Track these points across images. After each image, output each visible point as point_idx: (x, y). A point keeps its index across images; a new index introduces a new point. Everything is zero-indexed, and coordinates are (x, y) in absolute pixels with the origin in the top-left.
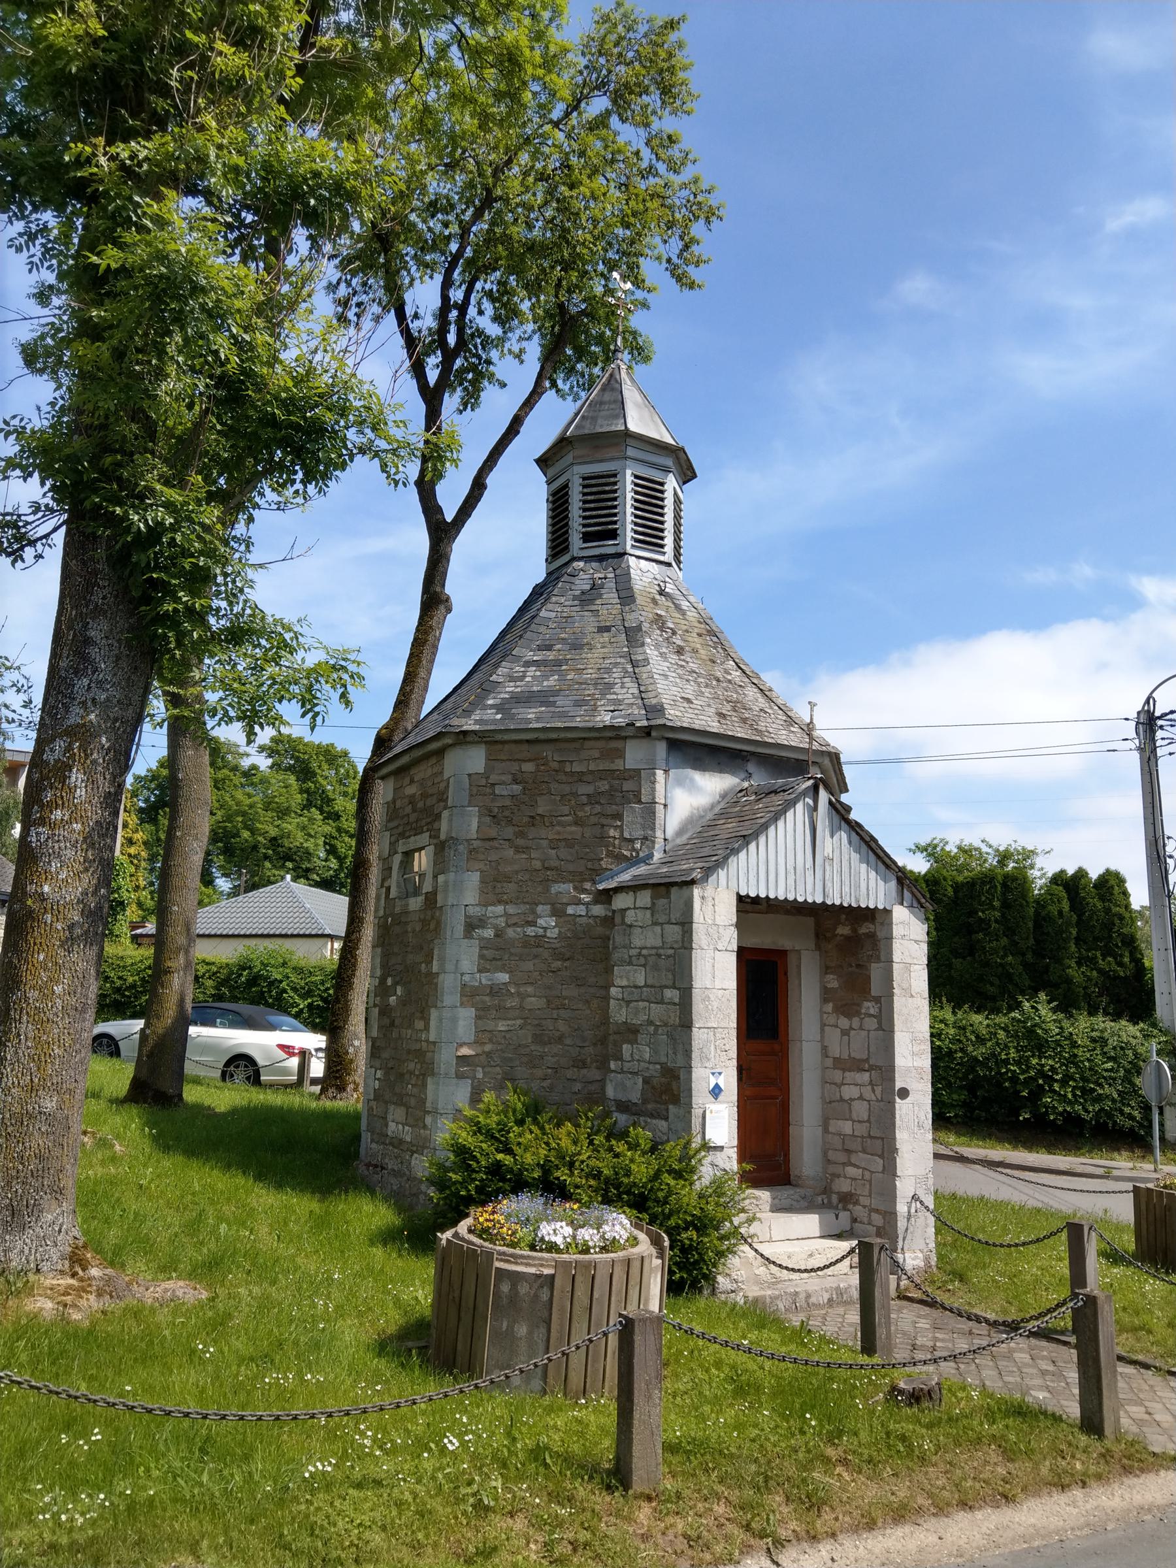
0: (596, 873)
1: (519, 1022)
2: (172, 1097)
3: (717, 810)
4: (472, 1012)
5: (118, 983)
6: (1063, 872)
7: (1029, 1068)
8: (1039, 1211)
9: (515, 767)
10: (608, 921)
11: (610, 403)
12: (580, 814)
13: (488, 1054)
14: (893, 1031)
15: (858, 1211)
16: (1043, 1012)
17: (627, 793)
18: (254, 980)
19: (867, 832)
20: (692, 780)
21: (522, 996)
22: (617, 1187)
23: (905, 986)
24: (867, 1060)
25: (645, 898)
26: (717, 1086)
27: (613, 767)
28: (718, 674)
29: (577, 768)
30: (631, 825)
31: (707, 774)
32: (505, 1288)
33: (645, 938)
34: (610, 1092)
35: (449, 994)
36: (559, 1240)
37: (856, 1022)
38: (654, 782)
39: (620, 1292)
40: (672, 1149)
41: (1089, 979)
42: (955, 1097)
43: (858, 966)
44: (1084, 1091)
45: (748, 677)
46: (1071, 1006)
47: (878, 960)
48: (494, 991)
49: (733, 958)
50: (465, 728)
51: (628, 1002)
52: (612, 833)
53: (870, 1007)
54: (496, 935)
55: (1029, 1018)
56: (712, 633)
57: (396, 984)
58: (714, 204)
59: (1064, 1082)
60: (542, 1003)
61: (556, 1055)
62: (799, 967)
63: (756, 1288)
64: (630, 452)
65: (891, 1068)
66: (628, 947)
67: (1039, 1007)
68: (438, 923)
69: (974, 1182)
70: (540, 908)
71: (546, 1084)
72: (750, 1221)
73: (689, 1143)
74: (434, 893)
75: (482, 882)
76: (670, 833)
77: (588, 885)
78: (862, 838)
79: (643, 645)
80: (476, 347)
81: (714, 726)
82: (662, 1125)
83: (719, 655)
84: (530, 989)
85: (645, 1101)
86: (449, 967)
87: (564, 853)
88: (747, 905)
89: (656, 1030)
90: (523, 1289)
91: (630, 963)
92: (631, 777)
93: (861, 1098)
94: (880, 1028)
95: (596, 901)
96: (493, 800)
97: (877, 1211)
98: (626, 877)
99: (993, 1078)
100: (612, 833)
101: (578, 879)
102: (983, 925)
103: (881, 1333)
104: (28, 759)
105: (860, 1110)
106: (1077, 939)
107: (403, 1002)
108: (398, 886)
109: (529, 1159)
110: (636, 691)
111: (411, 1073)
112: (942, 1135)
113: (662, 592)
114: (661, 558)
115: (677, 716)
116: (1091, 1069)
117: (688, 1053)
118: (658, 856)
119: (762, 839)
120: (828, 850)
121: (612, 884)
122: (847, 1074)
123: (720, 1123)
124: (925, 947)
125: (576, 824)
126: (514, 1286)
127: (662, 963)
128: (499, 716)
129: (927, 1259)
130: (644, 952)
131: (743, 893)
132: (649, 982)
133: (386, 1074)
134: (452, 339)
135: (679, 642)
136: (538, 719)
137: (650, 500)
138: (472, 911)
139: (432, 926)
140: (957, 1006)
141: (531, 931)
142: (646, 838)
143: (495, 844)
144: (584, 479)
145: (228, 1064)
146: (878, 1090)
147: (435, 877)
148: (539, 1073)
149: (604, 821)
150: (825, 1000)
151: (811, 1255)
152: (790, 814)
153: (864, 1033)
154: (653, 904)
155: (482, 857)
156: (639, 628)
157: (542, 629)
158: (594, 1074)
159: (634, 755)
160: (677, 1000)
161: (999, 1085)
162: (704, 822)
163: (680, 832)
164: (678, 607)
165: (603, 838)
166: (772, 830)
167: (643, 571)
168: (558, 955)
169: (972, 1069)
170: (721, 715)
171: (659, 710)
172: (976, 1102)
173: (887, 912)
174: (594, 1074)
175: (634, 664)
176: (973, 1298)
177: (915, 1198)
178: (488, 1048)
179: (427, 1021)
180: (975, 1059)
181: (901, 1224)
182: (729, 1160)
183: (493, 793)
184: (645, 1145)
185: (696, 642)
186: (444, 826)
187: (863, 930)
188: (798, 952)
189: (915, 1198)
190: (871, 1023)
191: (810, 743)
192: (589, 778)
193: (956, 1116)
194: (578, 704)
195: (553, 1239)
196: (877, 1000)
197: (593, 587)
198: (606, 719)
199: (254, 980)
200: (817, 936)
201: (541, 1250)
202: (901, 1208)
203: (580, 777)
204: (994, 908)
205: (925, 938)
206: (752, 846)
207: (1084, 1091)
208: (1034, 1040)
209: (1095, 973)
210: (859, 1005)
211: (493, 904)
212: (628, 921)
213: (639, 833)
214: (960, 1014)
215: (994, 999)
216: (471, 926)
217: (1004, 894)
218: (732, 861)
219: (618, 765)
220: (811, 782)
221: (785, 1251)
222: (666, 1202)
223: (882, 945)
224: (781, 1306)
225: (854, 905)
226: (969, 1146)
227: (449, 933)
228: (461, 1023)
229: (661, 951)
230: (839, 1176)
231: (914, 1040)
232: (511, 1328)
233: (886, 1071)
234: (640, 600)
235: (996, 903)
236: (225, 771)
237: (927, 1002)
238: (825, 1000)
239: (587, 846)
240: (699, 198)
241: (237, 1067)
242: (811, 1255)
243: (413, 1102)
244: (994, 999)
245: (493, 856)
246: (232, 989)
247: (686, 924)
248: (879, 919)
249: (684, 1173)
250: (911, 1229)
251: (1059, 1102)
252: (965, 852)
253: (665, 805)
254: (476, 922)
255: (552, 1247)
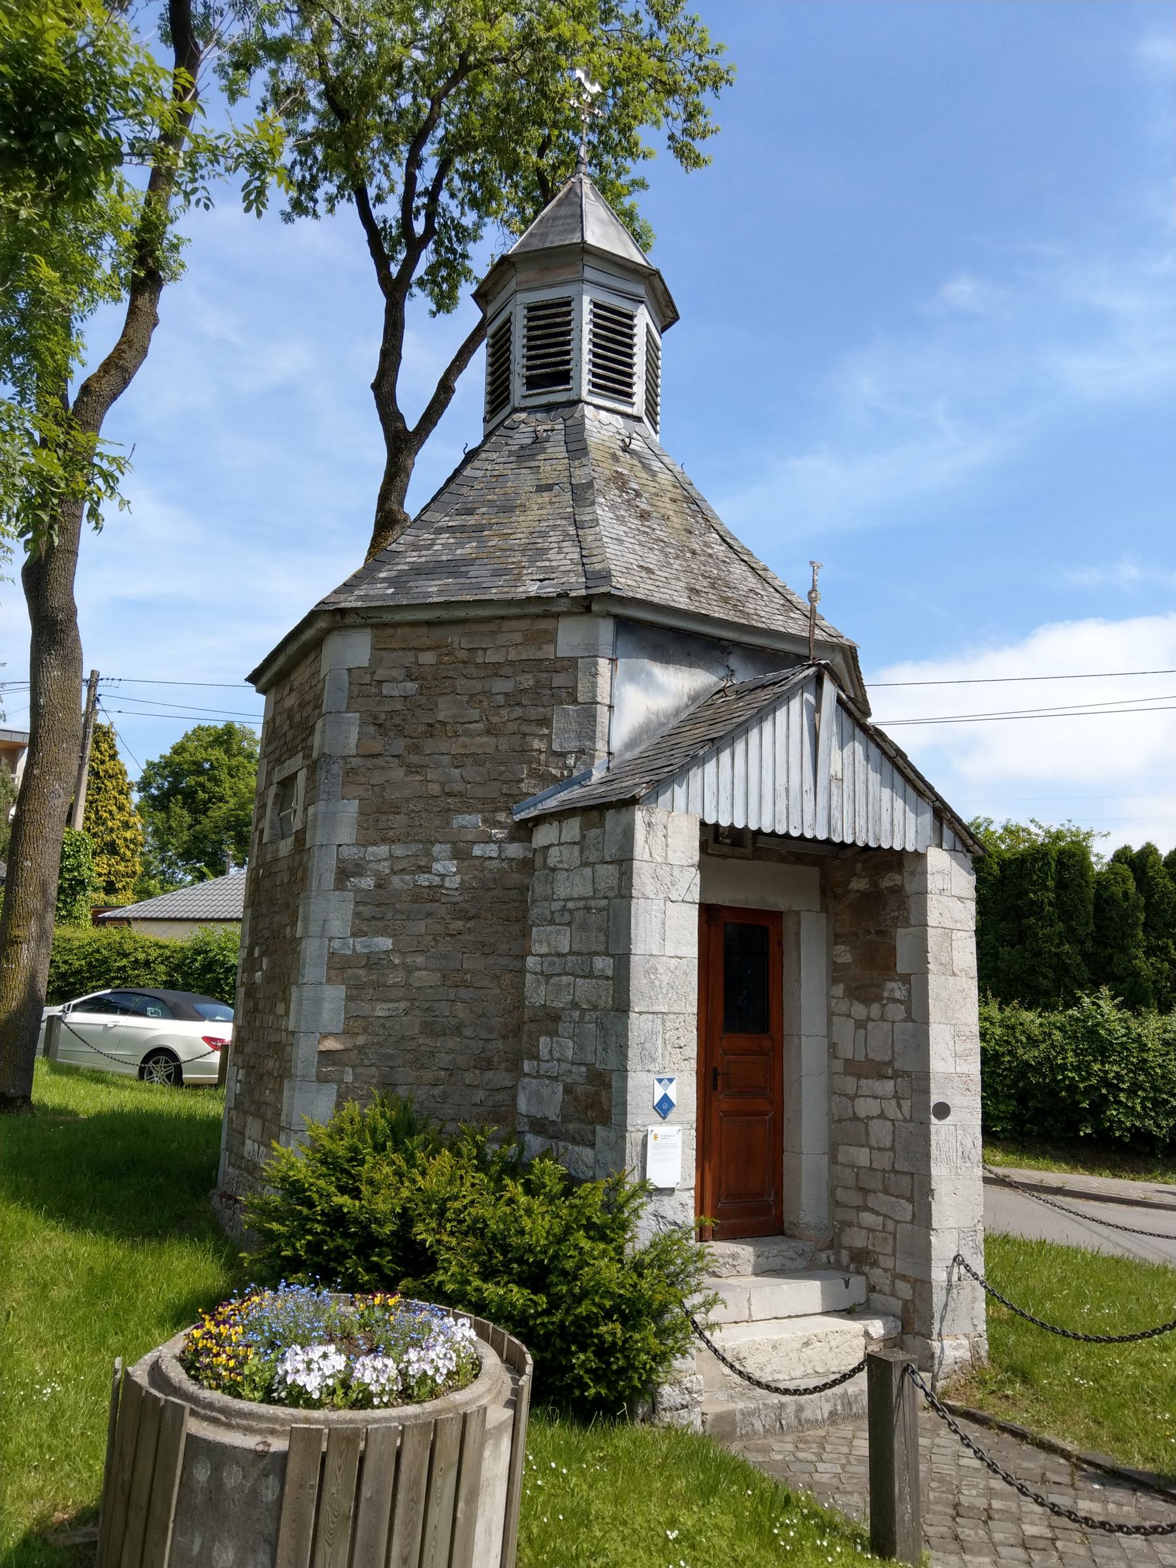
0: (513, 799)
1: (403, 1005)
2: (13, 1099)
3: (683, 716)
4: (339, 991)
5: (63, 968)
6: (1126, 849)
7: (1089, 1074)
8: (1118, 1261)
9: (408, 658)
10: (527, 865)
11: (565, 217)
12: (495, 720)
13: (361, 1049)
14: (927, 1023)
15: (877, 1275)
16: (1106, 1010)
17: (561, 690)
18: (209, 966)
19: (892, 744)
20: (649, 675)
21: (410, 969)
22: (505, 1249)
23: (944, 960)
24: (891, 1063)
25: (572, 829)
26: (665, 1098)
27: (540, 655)
28: (696, 547)
29: (492, 657)
30: (563, 736)
31: (671, 669)
32: (202, 1474)
33: (571, 886)
34: (523, 1105)
35: (313, 969)
36: (311, 1383)
37: (875, 1009)
38: (595, 675)
39: (416, 1482)
40: (593, 1196)
41: (1160, 972)
42: (1003, 1107)
43: (880, 933)
44: (1155, 1101)
45: (736, 552)
46: (1139, 1003)
47: (907, 923)
48: (373, 962)
49: (694, 912)
50: (343, 605)
51: (549, 977)
52: (537, 744)
53: (894, 988)
54: (378, 886)
55: (1090, 1016)
56: (691, 500)
57: (262, 954)
58: (723, 67)
59: (1132, 1092)
60: (434, 978)
61: (452, 1051)
62: (798, 934)
63: (722, 1396)
64: (589, 273)
65: (925, 1075)
66: (549, 899)
67: (1101, 1003)
68: (306, 869)
69: (1034, 1221)
70: (437, 848)
71: (436, 1091)
72: (708, 1304)
73: (619, 1183)
74: (303, 831)
75: (361, 813)
76: (617, 744)
77: (502, 817)
78: (884, 753)
79: (593, 503)
80: (450, 240)
81: (682, 602)
82: (587, 1153)
83: (699, 527)
84: (420, 960)
85: (566, 1119)
86: (314, 928)
87: (471, 773)
88: (719, 843)
89: (582, 1016)
90: (232, 1478)
91: (552, 922)
92: (565, 669)
93: (882, 1116)
94: (909, 1018)
95: (512, 839)
96: (379, 703)
97: (904, 1278)
98: (551, 804)
99: (1048, 1085)
100: (537, 744)
101: (490, 808)
102: (1035, 908)
103: (903, 1511)
104: (27, 740)
105: (881, 1133)
106: (1146, 926)
107: (269, 979)
108: (272, 828)
109: (382, 1205)
110: (576, 556)
111: (270, 1073)
112: (988, 1151)
113: (626, 449)
114: (628, 410)
115: (625, 583)
116: (1163, 1077)
117: (622, 1050)
118: (597, 775)
119: (740, 747)
120: (836, 768)
121: (533, 813)
122: (863, 1082)
123: (668, 1155)
124: (972, 906)
125: (488, 732)
126: (216, 1469)
127: (592, 919)
128: (391, 591)
129: (974, 1348)
130: (570, 905)
131: (710, 820)
132: (576, 948)
133: (248, 1075)
134: (419, 226)
135: (644, 506)
136: (440, 592)
137: (614, 333)
138: (346, 852)
139: (299, 876)
140: (1004, 1002)
141: (423, 880)
142: (582, 751)
143: (380, 761)
144: (530, 309)
145: (146, 1060)
146: (906, 1105)
147: (306, 809)
148: (428, 1075)
149: (526, 728)
150: (834, 981)
151: (807, 1344)
152: (781, 714)
153: (886, 1026)
154: (583, 836)
155: (362, 780)
156: (590, 485)
157: (465, 490)
158: (502, 1078)
159: (569, 638)
160: (610, 973)
161: (1054, 1094)
162: (666, 731)
163: (630, 745)
164: (646, 468)
165: (523, 752)
166: (754, 735)
167: (601, 422)
168: (459, 913)
169: (1023, 1075)
170: (693, 591)
171: (606, 576)
172: (1033, 1115)
173: (920, 857)
174: (502, 1078)
175: (578, 525)
176: (1042, 1411)
177: (958, 1260)
178: (361, 1040)
179: (286, 1000)
180: (1027, 1064)
181: (938, 1298)
182: (683, 1210)
183: (380, 694)
184: (553, 1185)
185: (669, 508)
186: (317, 740)
187: (886, 883)
188: (797, 913)
189: (958, 1260)
190: (897, 1012)
191: (811, 631)
192: (507, 671)
193: (1003, 1130)
194: (496, 574)
195: (301, 1380)
196: (906, 979)
197: (536, 440)
198: (533, 589)
199: (209, 966)
200: (824, 892)
201: (279, 1402)
202: (939, 1275)
203: (496, 671)
204: (1046, 888)
205: (973, 894)
206: (725, 756)
207: (1155, 1101)
208: (1095, 1042)
209: (1166, 965)
210: (880, 987)
211: (375, 844)
212: (551, 862)
213: (572, 745)
214: (1008, 1011)
215: (1047, 994)
216: (345, 873)
217: (1059, 872)
218: (695, 774)
219: (547, 652)
220: (811, 671)
221: (768, 1335)
222: (576, 1278)
223: (912, 903)
224: (758, 1426)
225: (872, 844)
226: (1019, 1166)
227: (315, 883)
228: (327, 1006)
229: (592, 903)
230: (851, 1225)
231: (956, 1035)
232: (206, 1549)
233: (920, 1079)
234: (594, 454)
235: (1050, 883)
236: (241, 759)
237: (975, 983)
238: (834, 981)
239: (501, 763)
240: (706, 61)
241: (157, 1062)
242: (807, 1344)
243: (269, 1114)
244: (1047, 994)
245: (377, 779)
246: (185, 975)
247: (624, 862)
248: (908, 866)
249: (610, 1227)
250: (952, 1305)
251: (1126, 1115)
252: (1011, 832)
253: (611, 707)
254: (351, 868)
255: (298, 1397)
